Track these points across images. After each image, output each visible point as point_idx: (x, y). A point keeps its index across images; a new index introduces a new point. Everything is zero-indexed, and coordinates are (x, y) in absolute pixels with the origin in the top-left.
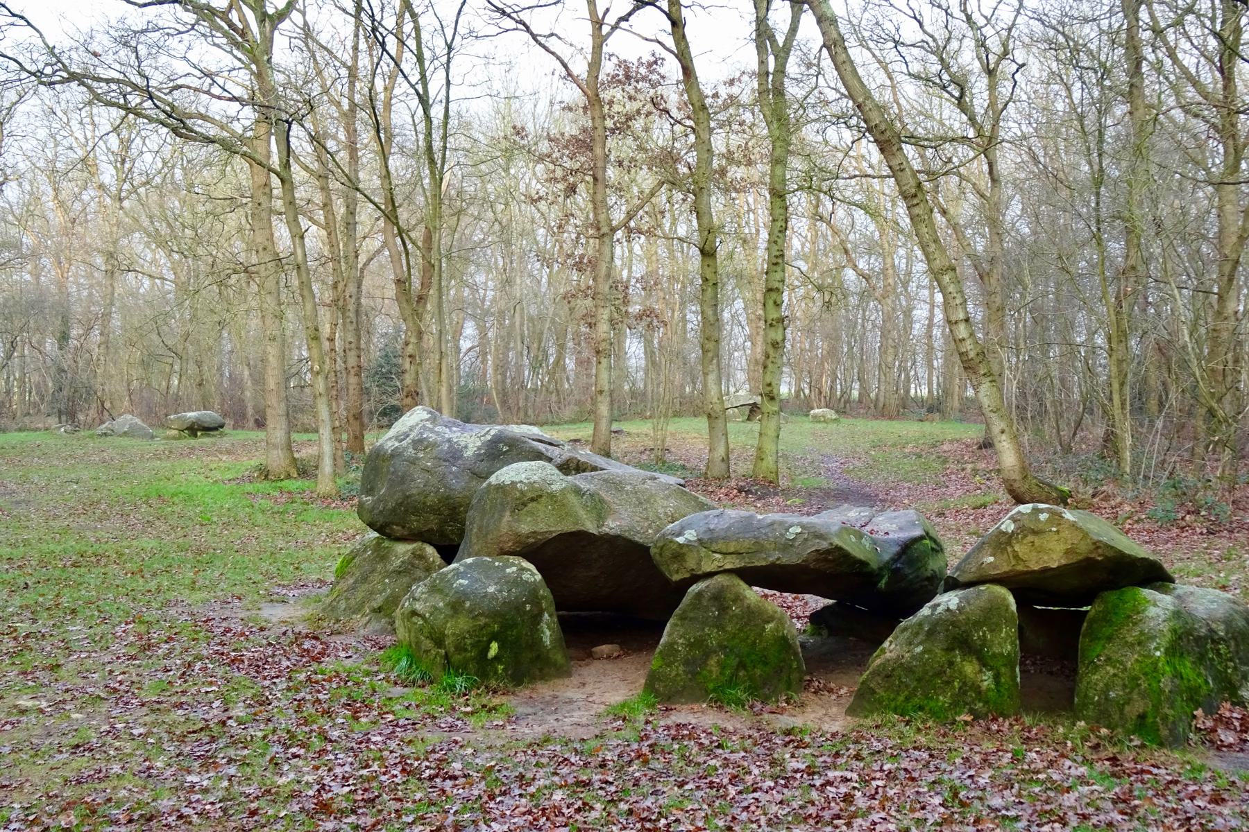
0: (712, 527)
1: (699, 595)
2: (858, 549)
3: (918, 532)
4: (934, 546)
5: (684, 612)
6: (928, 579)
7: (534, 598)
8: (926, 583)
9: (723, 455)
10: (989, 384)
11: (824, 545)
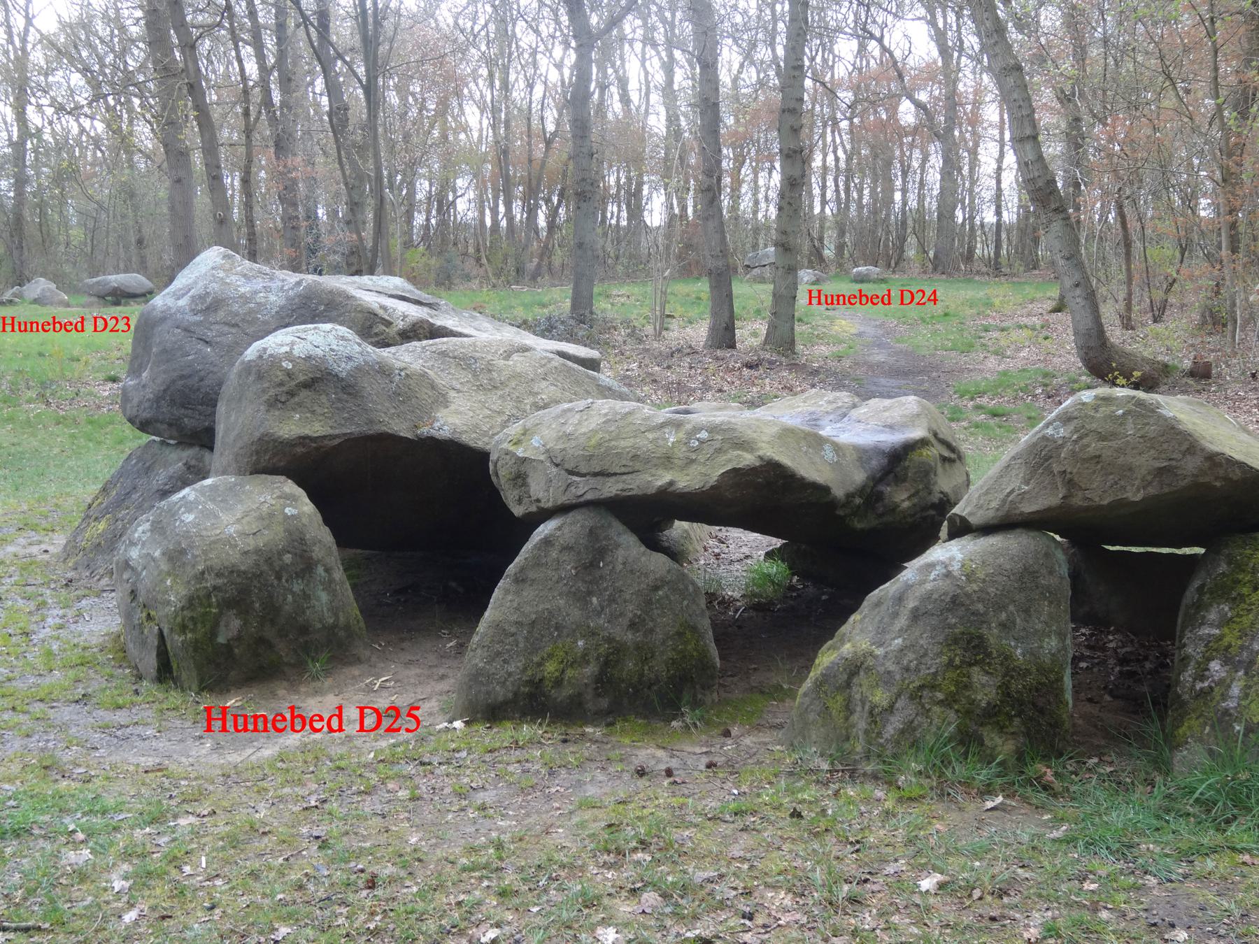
0: (569, 429)
1: (547, 542)
2: (811, 469)
3: (917, 433)
4: (946, 453)
5: (522, 569)
6: (933, 506)
7: (298, 542)
8: (932, 512)
9: (726, 320)
10: (1061, 222)
11: (747, 459)
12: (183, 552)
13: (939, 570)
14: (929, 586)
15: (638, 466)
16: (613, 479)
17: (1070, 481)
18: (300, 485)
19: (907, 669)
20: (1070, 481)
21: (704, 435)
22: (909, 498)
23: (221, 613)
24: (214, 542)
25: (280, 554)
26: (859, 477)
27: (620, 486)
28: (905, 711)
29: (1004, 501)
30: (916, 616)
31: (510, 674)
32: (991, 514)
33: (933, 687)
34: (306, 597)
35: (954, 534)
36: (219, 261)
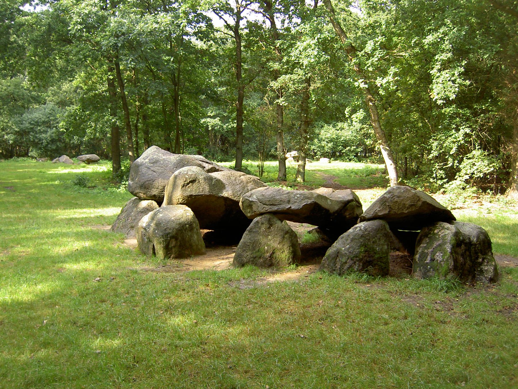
1: (257, 222)
5: (251, 229)
12: (160, 224)
13: (358, 229)
14: (356, 233)
15: (281, 203)
16: (275, 206)
17: (390, 207)
18: (189, 207)
19: (350, 253)
20: (390, 207)
21: (298, 196)
22: (349, 215)
23: (170, 240)
24: (169, 221)
25: (186, 224)
26: (336, 208)
27: (277, 208)
28: (350, 262)
29: (374, 212)
30: (352, 240)
31: (248, 255)
32: (371, 215)
33: (357, 257)
34: (191, 236)
35: (362, 221)
36: (155, 150)
